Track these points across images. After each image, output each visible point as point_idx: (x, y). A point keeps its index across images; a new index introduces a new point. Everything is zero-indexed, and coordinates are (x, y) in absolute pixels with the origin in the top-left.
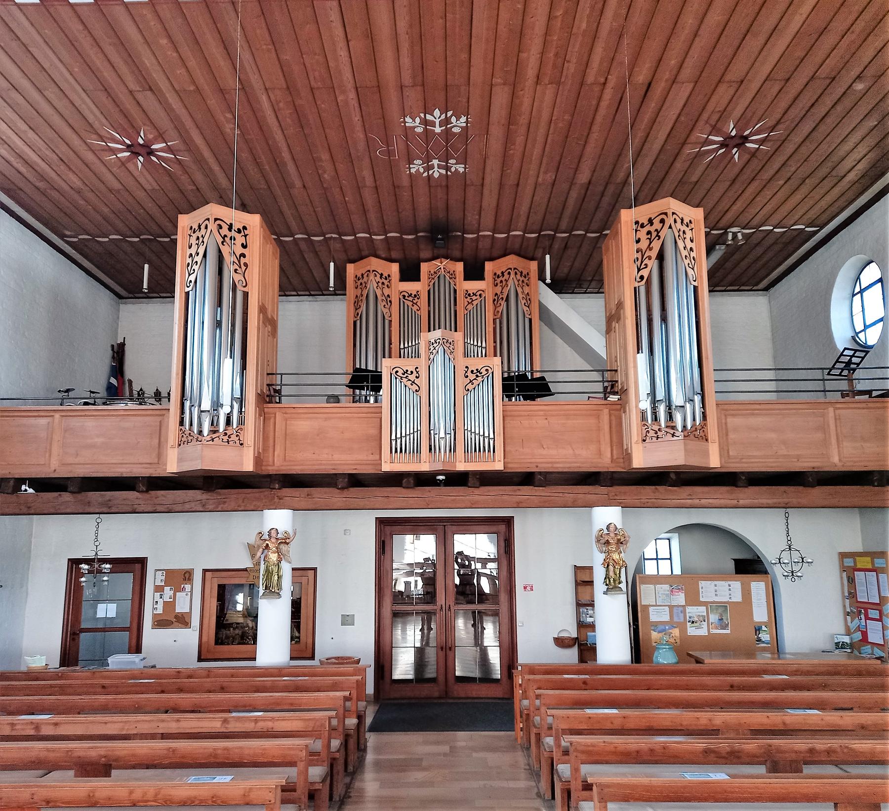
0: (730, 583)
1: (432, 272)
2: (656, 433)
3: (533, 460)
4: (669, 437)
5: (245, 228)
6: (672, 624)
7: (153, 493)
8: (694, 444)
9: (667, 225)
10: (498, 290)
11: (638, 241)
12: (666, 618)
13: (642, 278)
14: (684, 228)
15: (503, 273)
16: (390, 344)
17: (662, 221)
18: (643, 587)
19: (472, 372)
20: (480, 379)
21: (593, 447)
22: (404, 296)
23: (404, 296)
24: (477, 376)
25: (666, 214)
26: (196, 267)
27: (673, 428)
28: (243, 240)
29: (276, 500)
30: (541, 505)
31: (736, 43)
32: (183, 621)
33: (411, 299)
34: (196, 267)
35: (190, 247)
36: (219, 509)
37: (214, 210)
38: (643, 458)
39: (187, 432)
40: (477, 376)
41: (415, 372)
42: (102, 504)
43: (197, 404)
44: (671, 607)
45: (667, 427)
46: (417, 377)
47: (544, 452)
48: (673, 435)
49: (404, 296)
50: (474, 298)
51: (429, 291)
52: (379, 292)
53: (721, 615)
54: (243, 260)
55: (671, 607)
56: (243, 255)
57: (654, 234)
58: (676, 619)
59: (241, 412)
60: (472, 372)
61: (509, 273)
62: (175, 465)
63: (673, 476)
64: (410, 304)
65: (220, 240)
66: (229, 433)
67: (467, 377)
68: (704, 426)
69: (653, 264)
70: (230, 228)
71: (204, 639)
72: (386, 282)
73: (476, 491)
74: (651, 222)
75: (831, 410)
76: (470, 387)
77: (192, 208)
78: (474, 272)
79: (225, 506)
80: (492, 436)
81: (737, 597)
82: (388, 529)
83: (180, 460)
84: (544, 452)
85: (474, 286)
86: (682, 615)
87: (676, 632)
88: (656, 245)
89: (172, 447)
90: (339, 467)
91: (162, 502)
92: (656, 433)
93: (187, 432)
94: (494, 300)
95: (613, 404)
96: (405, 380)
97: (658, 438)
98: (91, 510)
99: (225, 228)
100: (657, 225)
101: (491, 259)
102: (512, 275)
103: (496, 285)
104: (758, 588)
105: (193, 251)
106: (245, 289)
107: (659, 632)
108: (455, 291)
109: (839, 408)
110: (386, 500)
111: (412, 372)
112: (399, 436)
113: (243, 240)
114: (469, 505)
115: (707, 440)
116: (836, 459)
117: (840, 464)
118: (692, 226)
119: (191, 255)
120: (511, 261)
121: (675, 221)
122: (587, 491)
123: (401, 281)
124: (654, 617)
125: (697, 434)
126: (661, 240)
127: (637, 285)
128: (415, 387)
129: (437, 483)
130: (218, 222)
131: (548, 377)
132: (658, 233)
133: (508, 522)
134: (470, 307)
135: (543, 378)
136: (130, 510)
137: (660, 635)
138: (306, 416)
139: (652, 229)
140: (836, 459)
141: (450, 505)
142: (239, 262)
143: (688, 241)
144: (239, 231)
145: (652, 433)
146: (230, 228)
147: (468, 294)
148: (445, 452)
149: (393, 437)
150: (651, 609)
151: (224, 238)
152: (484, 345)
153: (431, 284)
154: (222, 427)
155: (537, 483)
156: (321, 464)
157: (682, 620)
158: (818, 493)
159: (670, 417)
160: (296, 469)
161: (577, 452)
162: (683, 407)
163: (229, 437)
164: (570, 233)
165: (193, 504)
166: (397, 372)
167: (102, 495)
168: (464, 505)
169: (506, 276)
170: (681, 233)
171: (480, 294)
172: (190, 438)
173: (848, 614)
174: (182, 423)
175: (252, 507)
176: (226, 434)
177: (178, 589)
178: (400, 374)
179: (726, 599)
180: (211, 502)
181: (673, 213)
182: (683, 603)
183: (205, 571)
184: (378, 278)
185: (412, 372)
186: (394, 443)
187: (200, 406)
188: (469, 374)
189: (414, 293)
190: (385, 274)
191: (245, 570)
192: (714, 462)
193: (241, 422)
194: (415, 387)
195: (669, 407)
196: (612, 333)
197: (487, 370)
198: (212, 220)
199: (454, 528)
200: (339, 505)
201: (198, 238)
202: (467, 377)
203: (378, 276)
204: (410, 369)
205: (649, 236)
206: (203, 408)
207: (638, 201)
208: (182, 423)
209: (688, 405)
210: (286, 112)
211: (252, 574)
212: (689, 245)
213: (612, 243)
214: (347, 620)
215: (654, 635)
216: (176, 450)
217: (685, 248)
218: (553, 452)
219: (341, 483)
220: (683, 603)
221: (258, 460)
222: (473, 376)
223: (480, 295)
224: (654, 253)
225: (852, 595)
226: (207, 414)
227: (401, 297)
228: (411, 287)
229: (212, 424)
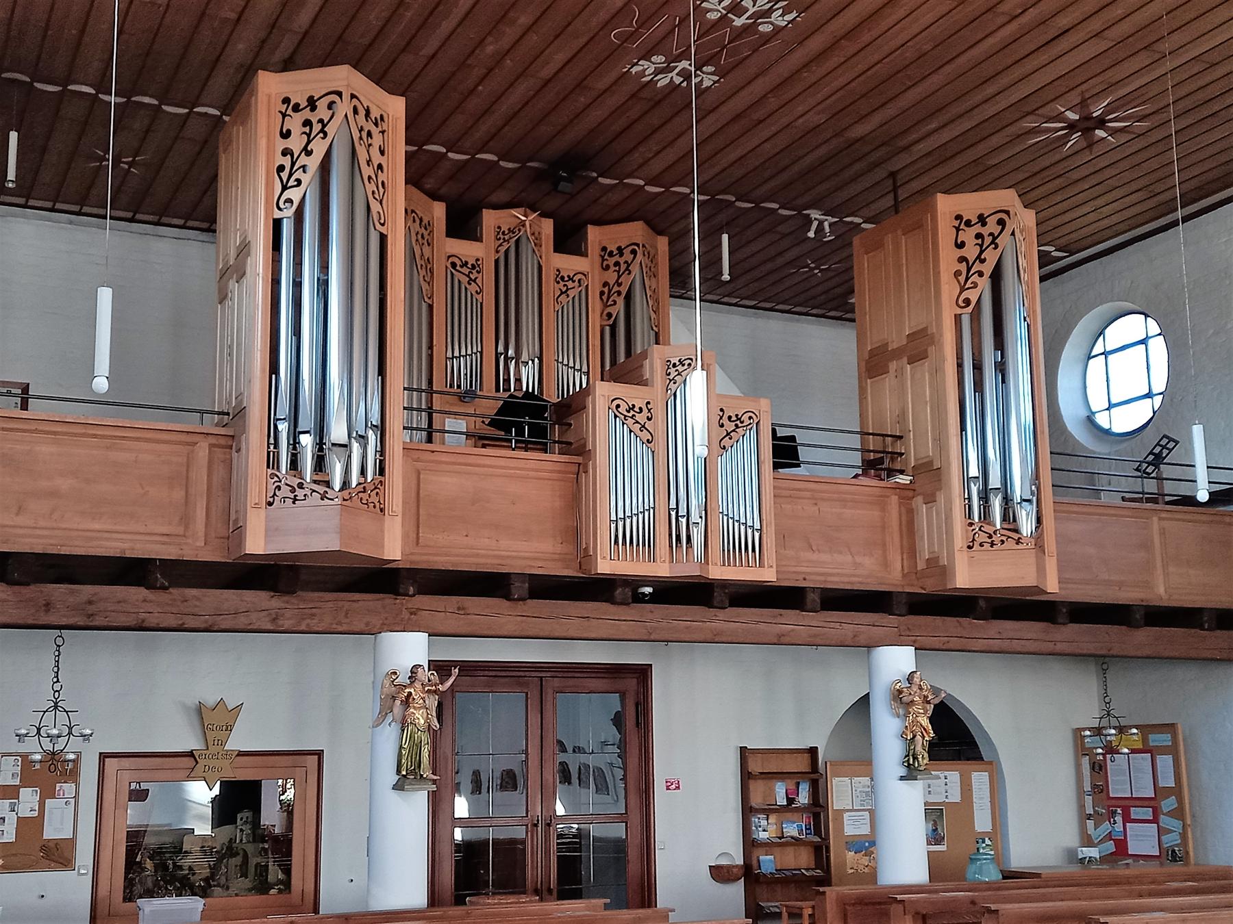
0: (947, 773)
1: (505, 228)
2: (293, 490)
4: (1010, 544)
9: (1008, 230)
10: (611, 277)
11: (960, 245)
13: (967, 302)
14: (370, 126)
15: (620, 249)
16: (431, 347)
17: (1001, 222)
18: (836, 781)
19: (730, 417)
22: (454, 265)
23: (454, 265)
25: (339, 94)
26: (306, 179)
27: (328, 484)
31: (1202, 11)
32: (58, 855)
36: (303, 627)
38: (967, 575)
40: (737, 426)
45: (315, 482)
46: (649, 419)
48: (1018, 542)
49: (455, 264)
50: (570, 284)
51: (497, 262)
53: (935, 824)
57: (317, 127)
60: (730, 417)
61: (634, 252)
62: (262, 544)
63: (982, 603)
64: (465, 280)
65: (356, 135)
67: (722, 426)
68: (379, 486)
69: (984, 284)
73: (721, 614)
74: (312, 103)
75: (1155, 519)
78: (569, 241)
79: (314, 623)
80: (757, 526)
81: (955, 797)
83: (270, 532)
84: (815, 557)
85: (569, 263)
88: (991, 257)
90: (829, 579)
91: (196, 610)
92: (293, 490)
94: (602, 293)
95: (903, 487)
97: (992, 544)
100: (992, 226)
101: (599, 222)
102: (639, 257)
103: (608, 267)
104: (980, 779)
109: (1164, 519)
110: (585, 622)
111: (641, 409)
112: (621, 515)
114: (709, 637)
116: (1161, 590)
117: (1165, 597)
120: (635, 231)
121: (355, 111)
123: (448, 236)
124: (850, 830)
125: (367, 496)
126: (1000, 249)
127: (959, 311)
129: (639, 599)
131: (801, 436)
132: (324, 126)
133: (642, 673)
135: (793, 438)
138: (451, 468)
139: (985, 231)
140: (1161, 590)
141: (683, 637)
143: (375, 152)
145: (285, 491)
147: (560, 278)
148: (638, 544)
150: (846, 815)
153: (503, 249)
155: (809, 606)
156: (477, 555)
159: (320, 463)
161: (859, 559)
162: (345, 446)
164: (65, 90)
165: (254, 616)
166: (618, 406)
168: (702, 638)
169: (628, 256)
170: (364, 135)
171: (577, 278)
173: (1089, 817)
177: (48, 793)
179: (940, 799)
180: (288, 614)
181: (353, 96)
183: (103, 756)
188: (725, 421)
189: (471, 262)
191: (191, 754)
192: (393, 548)
195: (320, 445)
196: (228, 303)
199: (556, 682)
200: (510, 628)
202: (722, 426)
205: (307, 129)
207: (287, 65)
209: (355, 446)
212: (377, 159)
213: (238, 132)
216: (262, 513)
217: (369, 162)
218: (825, 557)
222: (731, 426)
224: (988, 268)
225: (1100, 789)
228: (465, 249)
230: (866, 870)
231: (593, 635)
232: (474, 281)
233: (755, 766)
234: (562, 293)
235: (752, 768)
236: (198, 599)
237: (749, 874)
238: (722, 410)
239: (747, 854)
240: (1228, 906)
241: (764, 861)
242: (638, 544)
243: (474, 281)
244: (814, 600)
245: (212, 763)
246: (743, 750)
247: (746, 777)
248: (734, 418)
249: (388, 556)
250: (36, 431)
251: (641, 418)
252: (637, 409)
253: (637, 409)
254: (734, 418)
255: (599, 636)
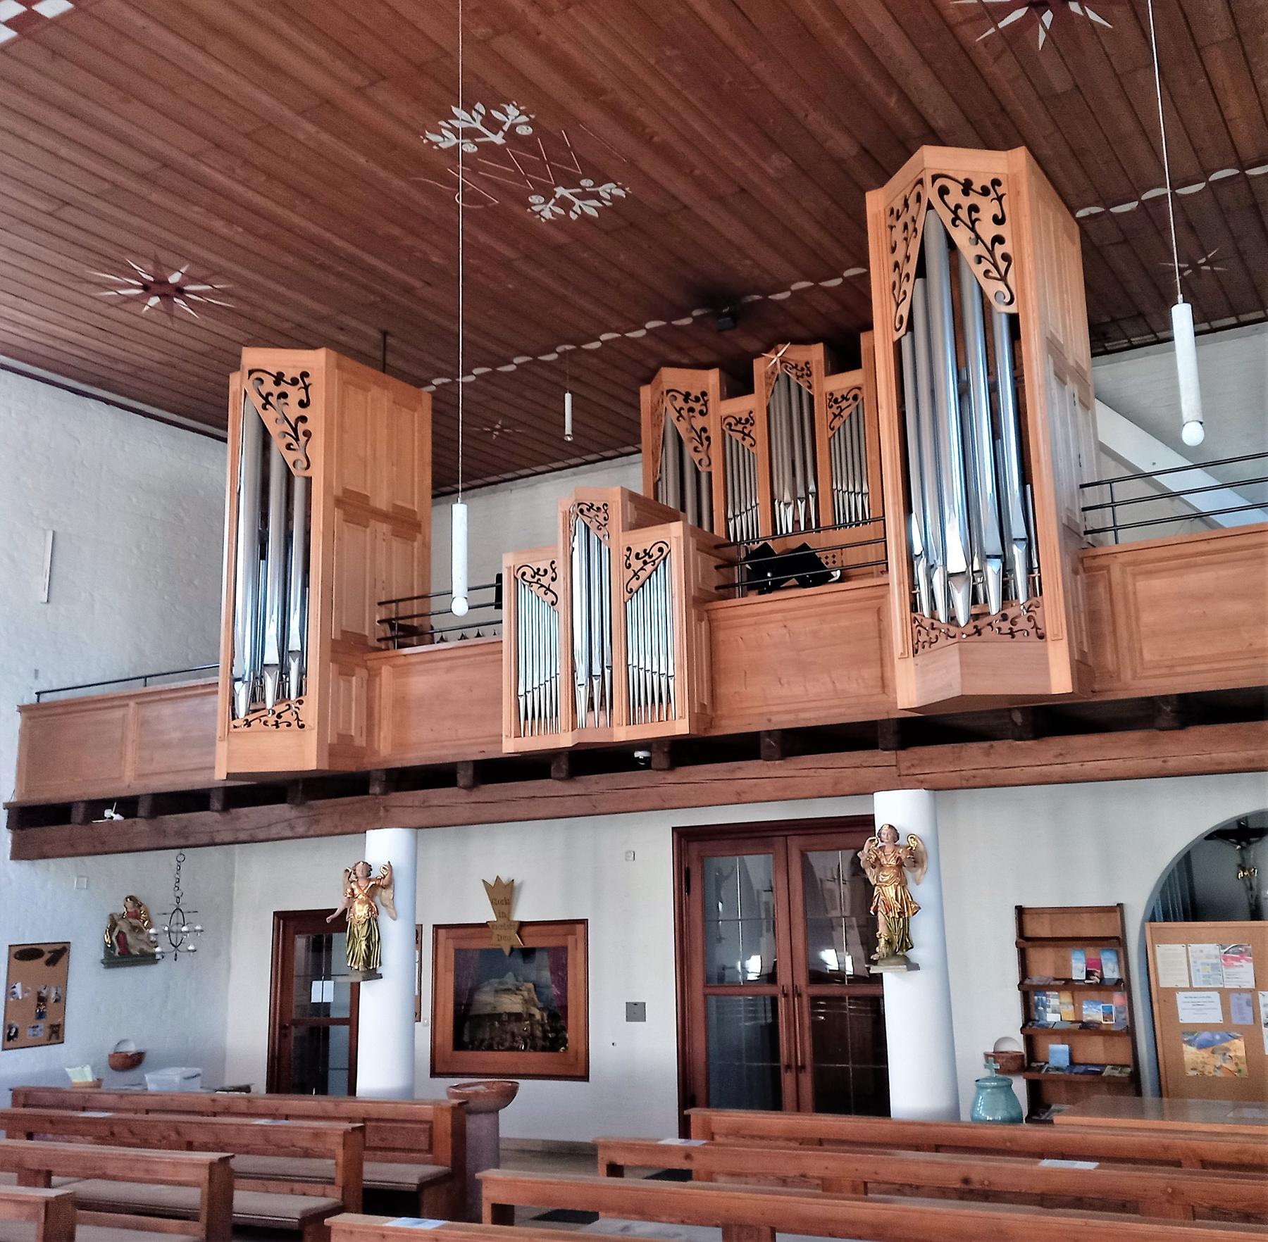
3: (765, 709)
5: (305, 375)
6: (1226, 1029)
7: (234, 811)
8: (993, 649)
12: (1215, 1016)
20: (649, 567)
21: (870, 673)
22: (730, 424)
24: (645, 563)
28: (994, 208)
29: (382, 813)
30: (780, 794)
33: (740, 427)
34: (907, 286)
35: (893, 250)
36: (311, 832)
37: (932, 158)
39: (927, 623)
40: (645, 563)
41: (550, 571)
42: (178, 833)
43: (940, 562)
44: (1225, 993)
47: (785, 691)
52: (682, 427)
54: (301, 427)
55: (1225, 993)
56: (998, 239)
58: (1236, 1019)
59: (1030, 570)
66: (1011, 612)
67: (629, 567)
70: (967, 187)
71: (439, 1040)
72: (698, 407)
76: (634, 584)
77: (882, 176)
82: (694, 847)
86: (1248, 1011)
87: (1238, 1047)
89: (222, 740)
93: (927, 623)
96: (536, 586)
98: (167, 843)
99: (269, 381)
105: (899, 256)
106: (307, 473)
107: (1201, 1047)
108: (811, 398)
111: (546, 571)
113: (994, 208)
115: (1042, 637)
118: (1000, 190)
119: (896, 265)
122: (858, 762)
128: (551, 597)
129: (635, 765)
130: (255, 375)
134: (837, 423)
136: (206, 839)
137: (1205, 1053)
142: (295, 430)
144: (985, 192)
146: (967, 187)
147: (833, 400)
149: (521, 691)
150: (1180, 996)
151: (955, 212)
152: (865, 489)
154: (994, 607)
157: (1250, 1021)
158: (1005, 755)
160: (415, 757)
163: (1013, 622)
166: (524, 574)
167: (178, 819)
172: (933, 634)
174: (914, 607)
175: (353, 828)
176: (1004, 617)
178: (527, 577)
182: (1251, 985)
183: (437, 927)
184: (680, 403)
185: (546, 571)
186: (522, 700)
187: (945, 564)
189: (745, 416)
190: (696, 392)
193: (1035, 588)
194: (551, 597)
197: (661, 550)
198: (928, 181)
201: (906, 227)
202: (629, 567)
203: (680, 398)
204: (544, 565)
206: (951, 570)
208: (914, 607)
210: (279, 191)
211: (496, 932)
214: (636, 1012)
215: (1190, 1053)
216: (225, 744)
219: (464, 777)
220: (1251, 985)
221: (1082, 668)
222: (637, 565)
223: (855, 398)
226: (960, 579)
227: (726, 428)
228: (740, 406)
229: (975, 601)
230: (1219, 1074)
231: (540, 815)
232: (749, 435)
233: (1037, 929)
234: (835, 416)
235: (1033, 935)
236: (247, 816)
237: (1027, 1062)
238: (629, 549)
239: (1029, 1041)
240: (1249, 1216)
241: (1055, 1052)
242: (646, 703)
243: (749, 435)
244: (770, 746)
245: (502, 932)
246: (1020, 911)
247: (1026, 943)
248: (642, 555)
249: (1056, 690)
250: (186, 697)
251: (545, 581)
252: (542, 572)
253: (542, 572)
254: (642, 555)
255: (550, 814)
